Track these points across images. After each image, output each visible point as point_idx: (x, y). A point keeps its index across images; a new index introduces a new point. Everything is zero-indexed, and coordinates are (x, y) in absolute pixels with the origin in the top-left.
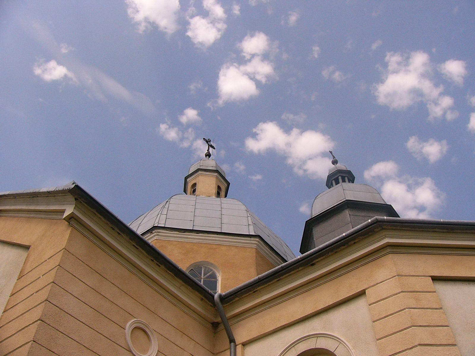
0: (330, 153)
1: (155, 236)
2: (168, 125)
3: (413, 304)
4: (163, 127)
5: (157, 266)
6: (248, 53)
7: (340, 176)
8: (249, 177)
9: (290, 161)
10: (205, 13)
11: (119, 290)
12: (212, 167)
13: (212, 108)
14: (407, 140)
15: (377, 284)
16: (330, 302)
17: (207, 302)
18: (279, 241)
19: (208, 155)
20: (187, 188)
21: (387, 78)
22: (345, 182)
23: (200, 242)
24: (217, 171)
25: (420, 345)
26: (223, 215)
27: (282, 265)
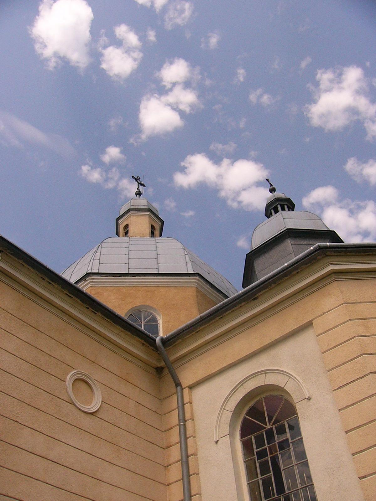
0: (267, 181)
1: (89, 283)
2: (90, 166)
3: (362, 331)
4: (85, 169)
5: (94, 314)
6: (168, 82)
7: (279, 204)
8: (182, 214)
9: (223, 194)
10: (118, 43)
11: (56, 342)
12: (144, 205)
13: (135, 144)
14: (345, 163)
15: (324, 313)
16: (277, 336)
17: (149, 347)
18: (220, 278)
19: (139, 194)
20: (120, 229)
21: (319, 97)
22: (285, 210)
23: (137, 286)
24: (149, 210)
25: (371, 373)
26: (159, 255)
27: (224, 301)
